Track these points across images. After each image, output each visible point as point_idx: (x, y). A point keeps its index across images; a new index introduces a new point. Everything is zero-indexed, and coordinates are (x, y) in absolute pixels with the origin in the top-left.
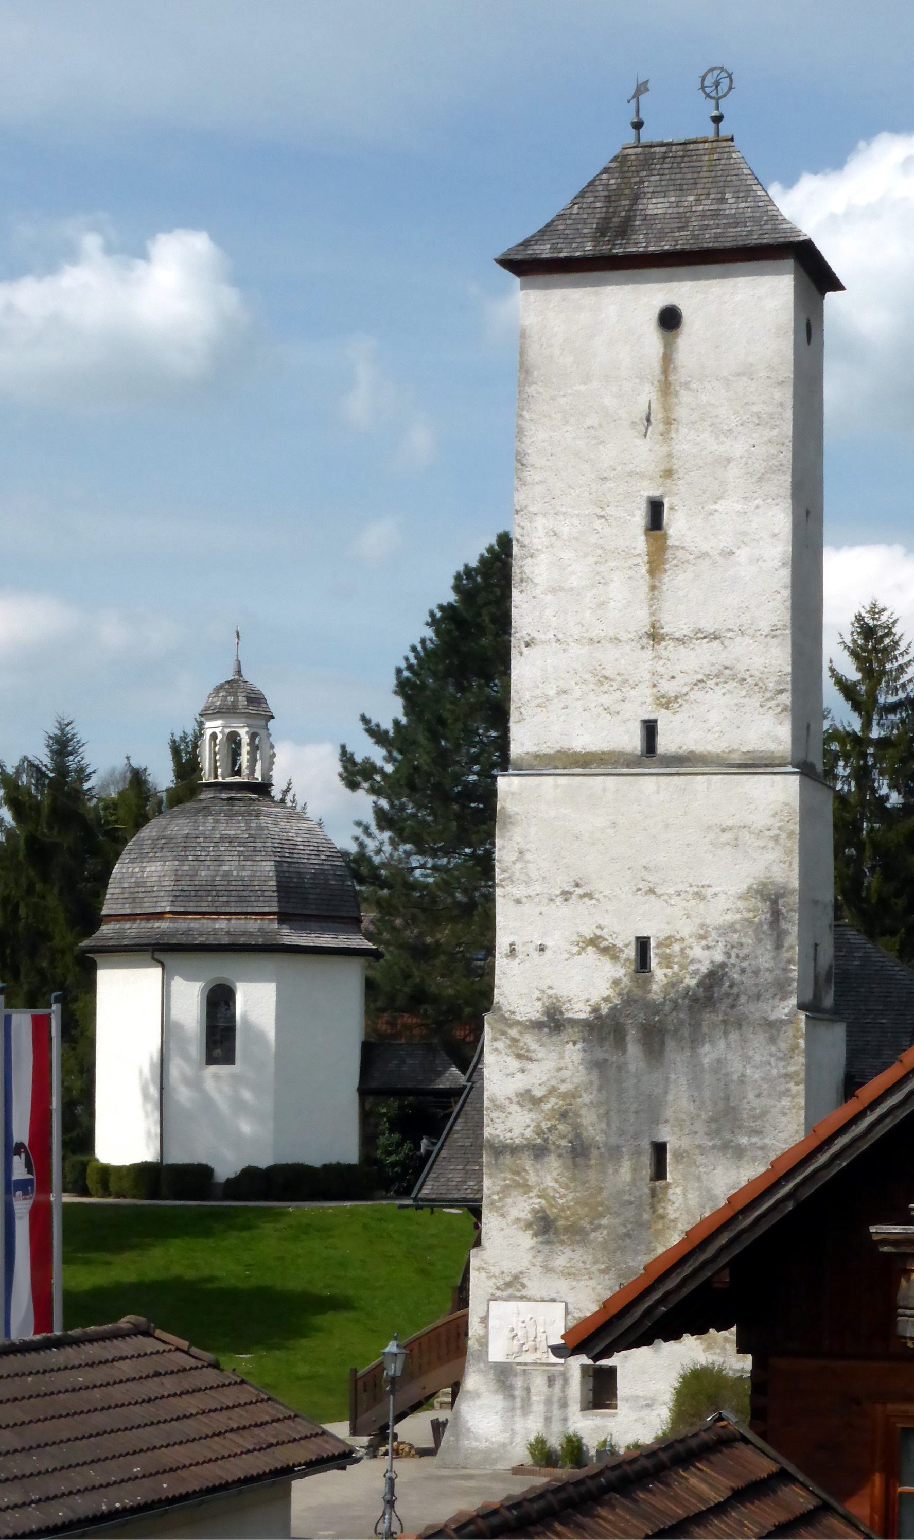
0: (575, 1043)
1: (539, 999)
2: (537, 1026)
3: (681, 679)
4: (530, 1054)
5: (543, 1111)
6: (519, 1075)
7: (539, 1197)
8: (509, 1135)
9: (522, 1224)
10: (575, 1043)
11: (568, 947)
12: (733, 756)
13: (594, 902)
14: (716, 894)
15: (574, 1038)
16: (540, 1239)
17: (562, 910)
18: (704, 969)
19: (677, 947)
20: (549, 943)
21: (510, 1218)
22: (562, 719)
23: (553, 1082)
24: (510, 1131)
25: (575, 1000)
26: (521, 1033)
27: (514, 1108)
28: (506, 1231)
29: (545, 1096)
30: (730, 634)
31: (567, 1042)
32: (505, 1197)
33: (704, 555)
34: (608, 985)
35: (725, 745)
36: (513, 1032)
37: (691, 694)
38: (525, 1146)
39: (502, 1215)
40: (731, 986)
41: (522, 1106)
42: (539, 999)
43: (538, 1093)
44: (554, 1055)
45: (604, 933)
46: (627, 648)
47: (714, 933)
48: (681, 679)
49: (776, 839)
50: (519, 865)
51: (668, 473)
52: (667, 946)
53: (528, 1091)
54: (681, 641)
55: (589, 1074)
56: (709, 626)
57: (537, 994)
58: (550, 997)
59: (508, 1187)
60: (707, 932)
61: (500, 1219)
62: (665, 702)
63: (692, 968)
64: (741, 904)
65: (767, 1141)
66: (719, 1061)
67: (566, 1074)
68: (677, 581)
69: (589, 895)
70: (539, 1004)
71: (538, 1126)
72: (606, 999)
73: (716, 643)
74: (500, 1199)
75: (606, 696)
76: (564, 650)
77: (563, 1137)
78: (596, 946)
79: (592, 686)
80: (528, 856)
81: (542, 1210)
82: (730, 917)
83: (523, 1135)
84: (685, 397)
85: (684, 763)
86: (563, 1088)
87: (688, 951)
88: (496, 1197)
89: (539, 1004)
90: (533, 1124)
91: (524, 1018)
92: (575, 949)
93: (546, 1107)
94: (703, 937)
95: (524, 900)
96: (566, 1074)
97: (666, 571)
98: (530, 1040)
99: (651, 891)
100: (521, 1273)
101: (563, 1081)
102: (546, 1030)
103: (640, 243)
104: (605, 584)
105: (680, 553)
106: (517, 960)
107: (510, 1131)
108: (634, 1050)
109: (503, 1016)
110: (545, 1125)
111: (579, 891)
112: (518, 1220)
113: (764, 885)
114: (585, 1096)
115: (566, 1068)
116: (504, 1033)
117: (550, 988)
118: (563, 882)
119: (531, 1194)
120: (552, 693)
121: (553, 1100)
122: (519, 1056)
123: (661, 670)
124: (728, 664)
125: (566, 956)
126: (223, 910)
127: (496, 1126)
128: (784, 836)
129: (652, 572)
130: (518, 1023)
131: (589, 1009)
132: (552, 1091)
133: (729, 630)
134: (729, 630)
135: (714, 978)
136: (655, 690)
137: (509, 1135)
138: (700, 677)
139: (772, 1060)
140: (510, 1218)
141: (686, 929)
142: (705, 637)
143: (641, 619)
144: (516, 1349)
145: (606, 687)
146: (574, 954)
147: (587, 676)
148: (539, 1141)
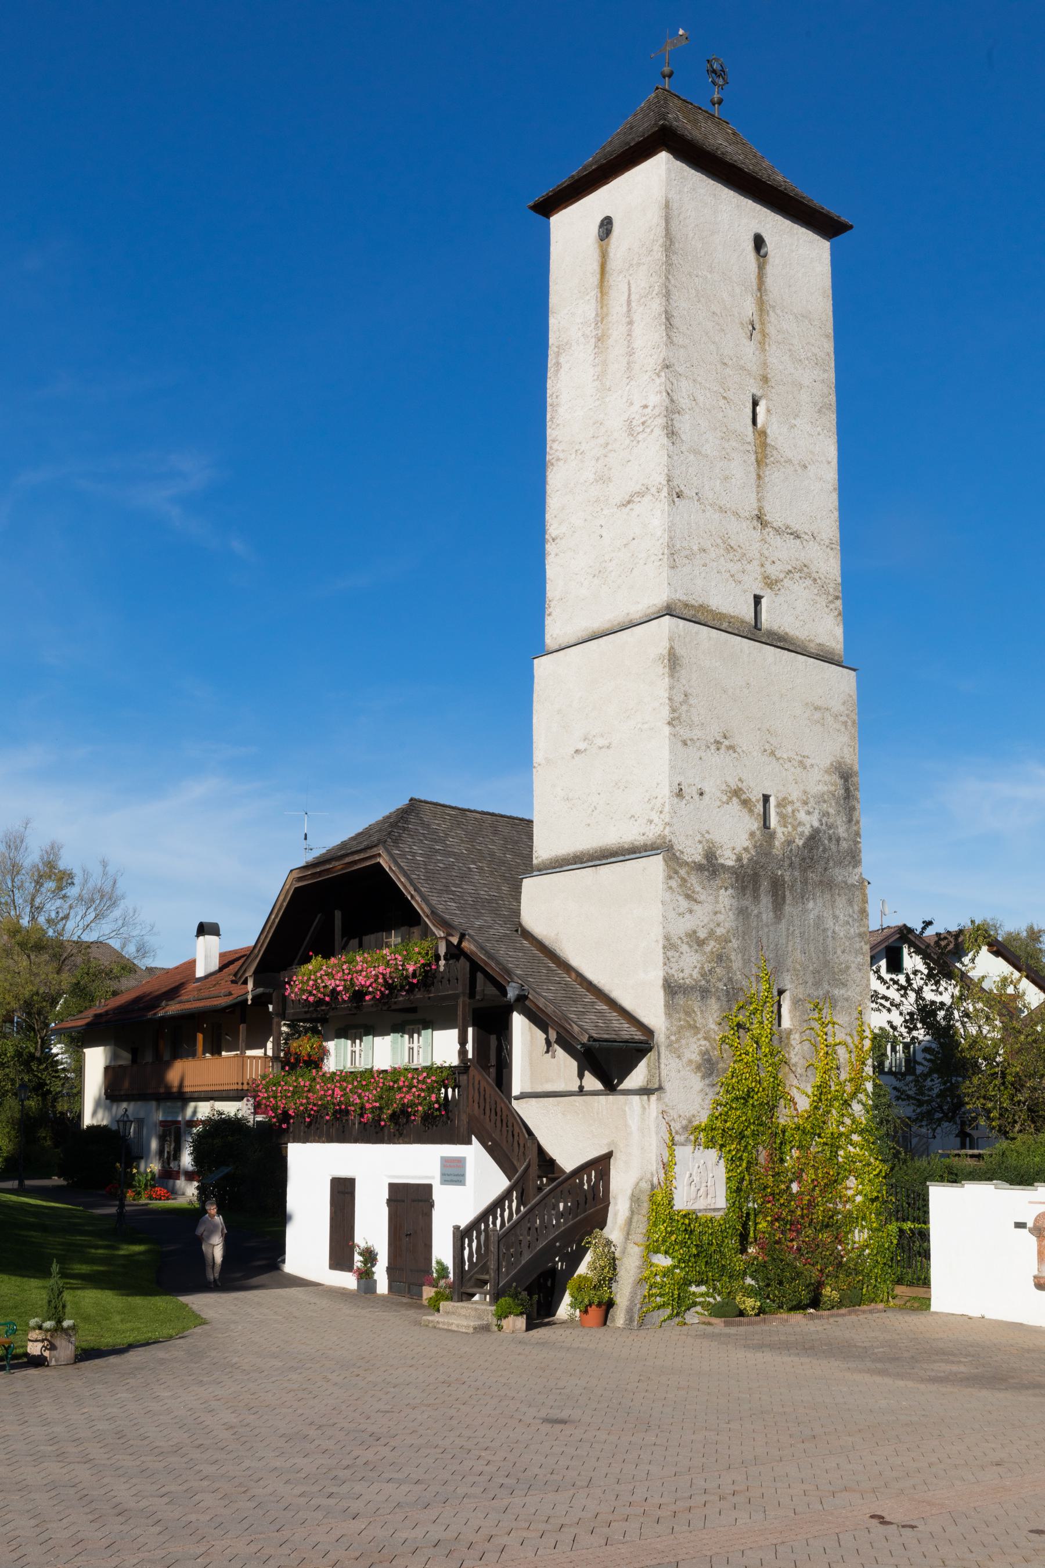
0: (726, 889)
1: (700, 842)
2: (699, 868)
3: (779, 566)
4: (696, 896)
5: (705, 953)
6: (688, 916)
7: (705, 1039)
8: (681, 975)
9: (693, 1066)
10: (726, 889)
11: (719, 794)
12: (812, 645)
13: (736, 755)
14: (812, 765)
15: (726, 885)
16: (707, 1081)
17: (716, 759)
18: (807, 831)
19: (789, 809)
20: (706, 789)
21: (685, 1060)
22: (703, 575)
23: (712, 926)
24: (682, 971)
25: (725, 847)
26: (688, 873)
27: (685, 948)
28: (682, 1073)
29: (706, 939)
30: (806, 537)
31: (721, 888)
32: (681, 1038)
33: (789, 461)
34: (747, 836)
35: (806, 633)
36: (683, 872)
37: (785, 580)
38: (692, 988)
39: (679, 1057)
40: (824, 851)
41: (691, 947)
42: (700, 842)
43: (702, 934)
44: (711, 898)
45: (743, 786)
46: (744, 525)
47: (812, 800)
48: (779, 566)
49: (845, 723)
50: (684, 708)
51: (765, 379)
52: (784, 807)
53: (695, 932)
54: (777, 530)
55: (737, 920)
56: (796, 527)
57: (698, 837)
58: (708, 841)
59: (681, 1027)
60: (808, 798)
61: (677, 1060)
62: (771, 583)
63: (800, 829)
64: (827, 778)
65: (849, 993)
66: (818, 917)
67: (721, 918)
68: (774, 475)
69: (731, 748)
70: (700, 846)
71: (703, 968)
72: (746, 849)
73: (798, 541)
74: (678, 1041)
75: (732, 564)
76: (704, 511)
77: (720, 980)
78: (738, 797)
79: (722, 551)
80: (692, 701)
81: (707, 1052)
82: (822, 788)
83: (691, 975)
84: (772, 317)
85: (780, 641)
86: (720, 931)
87: (796, 813)
88: (673, 1038)
89: (700, 846)
90: (699, 965)
91: (690, 860)
92: (725, 798)
93: (708, 949)
94: (806, 803)
95: (689, 742)
96: (721, 918)
97: (767, 465)
98: (694, 880)
99: (773, 753)
100: (694, 1116)
101: (718, 925)
102: (706, 873)
103: (552, 1195)
104: (729, 460)
105: (775, 452)
106: (684, 801)
107: (682, 971)
108: (766, 900)
109: (674, 854)
110: (707, 967)
111: (727, 743)
112: (690, 1061)
113: (840, 763)
114: (734, 941)
115: (720, 913)
116: (676, 872)
117: (708, 832)
118: (714, 731)
119: (699, 1036)
120: (695, 548)
121: (712, 943)
122: (688, 897)
123: (766, 553)
124: (806, 562)
125: (719, 803)
126: (774, 643)
127: (672, 965)
128: (850, 723)
129: (759, 462)
130: (687, 863)
131: (734, 857)
132: (711, 933)
133: (806, 533)
134: (806, 533)
135: (814, 838)
136: (763, 569)
137: (681, 975)
138: (790, 568)
139: (850, 920)
140: (685, 1060)
141: (795, 794)
142: (791, 534)
143: (750, 506)
144: (693, 1196)
145: (731, 556)
146: (724, 803)
147: (719, 541)
148: (703, 982)
